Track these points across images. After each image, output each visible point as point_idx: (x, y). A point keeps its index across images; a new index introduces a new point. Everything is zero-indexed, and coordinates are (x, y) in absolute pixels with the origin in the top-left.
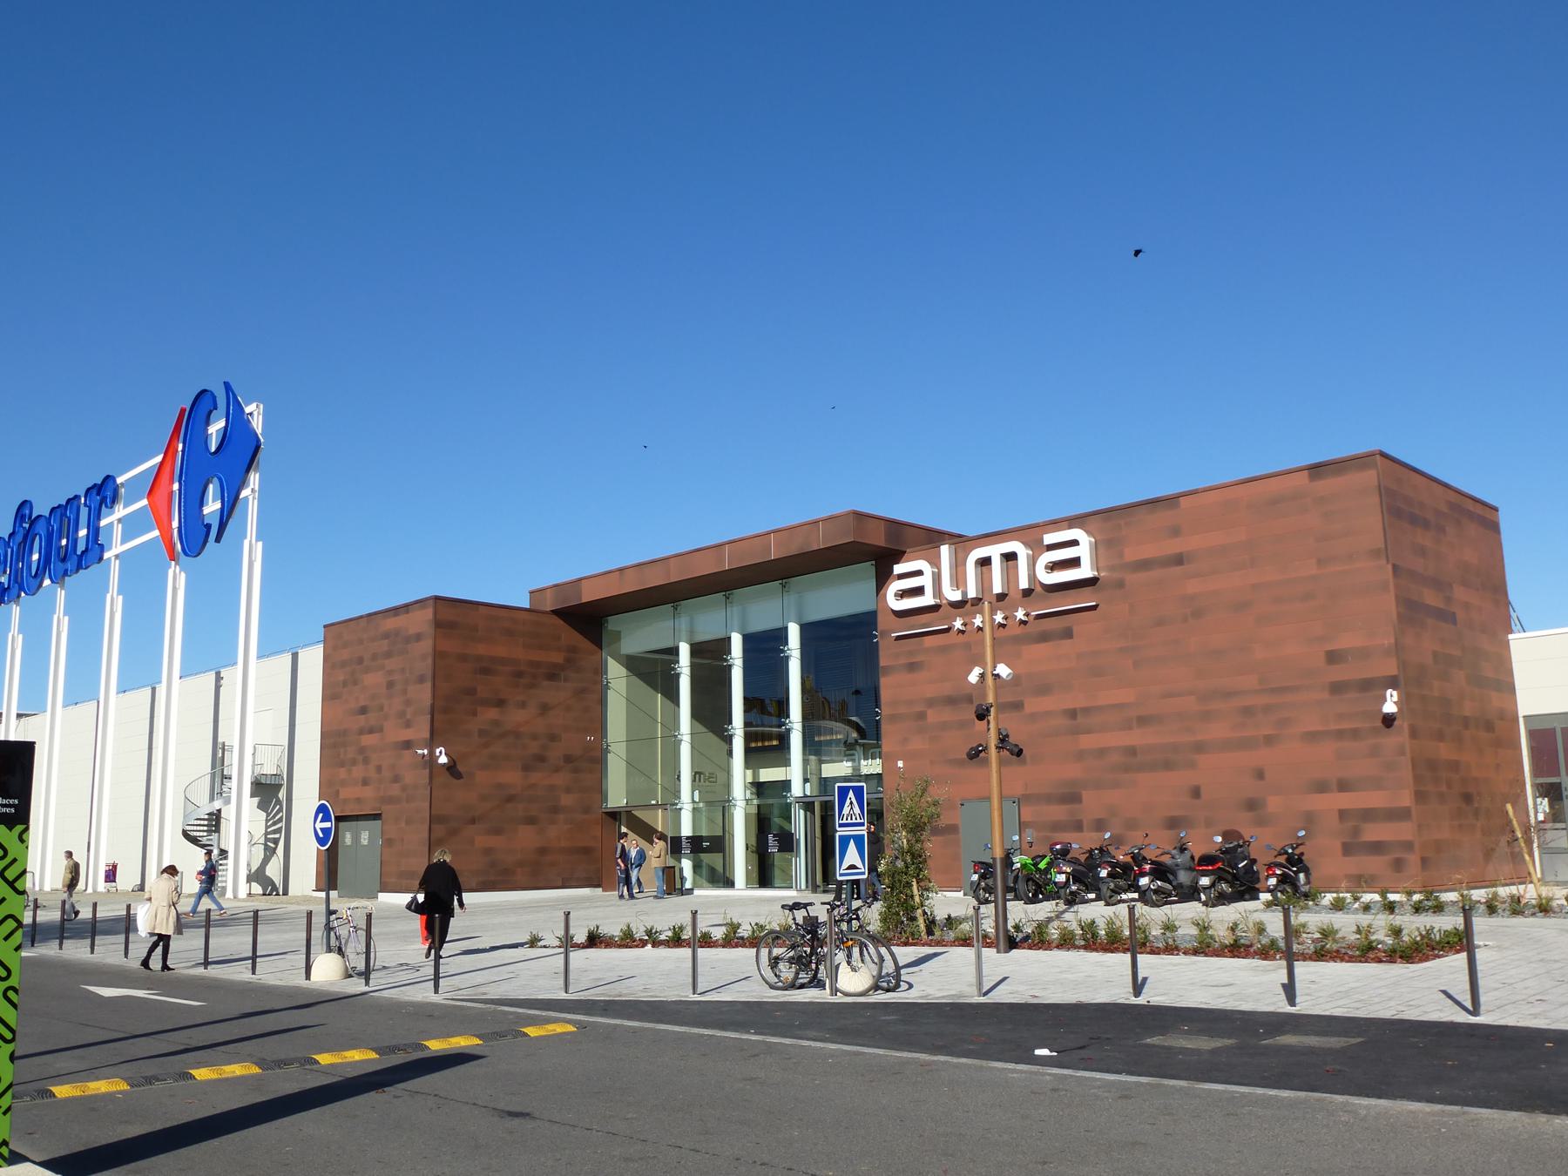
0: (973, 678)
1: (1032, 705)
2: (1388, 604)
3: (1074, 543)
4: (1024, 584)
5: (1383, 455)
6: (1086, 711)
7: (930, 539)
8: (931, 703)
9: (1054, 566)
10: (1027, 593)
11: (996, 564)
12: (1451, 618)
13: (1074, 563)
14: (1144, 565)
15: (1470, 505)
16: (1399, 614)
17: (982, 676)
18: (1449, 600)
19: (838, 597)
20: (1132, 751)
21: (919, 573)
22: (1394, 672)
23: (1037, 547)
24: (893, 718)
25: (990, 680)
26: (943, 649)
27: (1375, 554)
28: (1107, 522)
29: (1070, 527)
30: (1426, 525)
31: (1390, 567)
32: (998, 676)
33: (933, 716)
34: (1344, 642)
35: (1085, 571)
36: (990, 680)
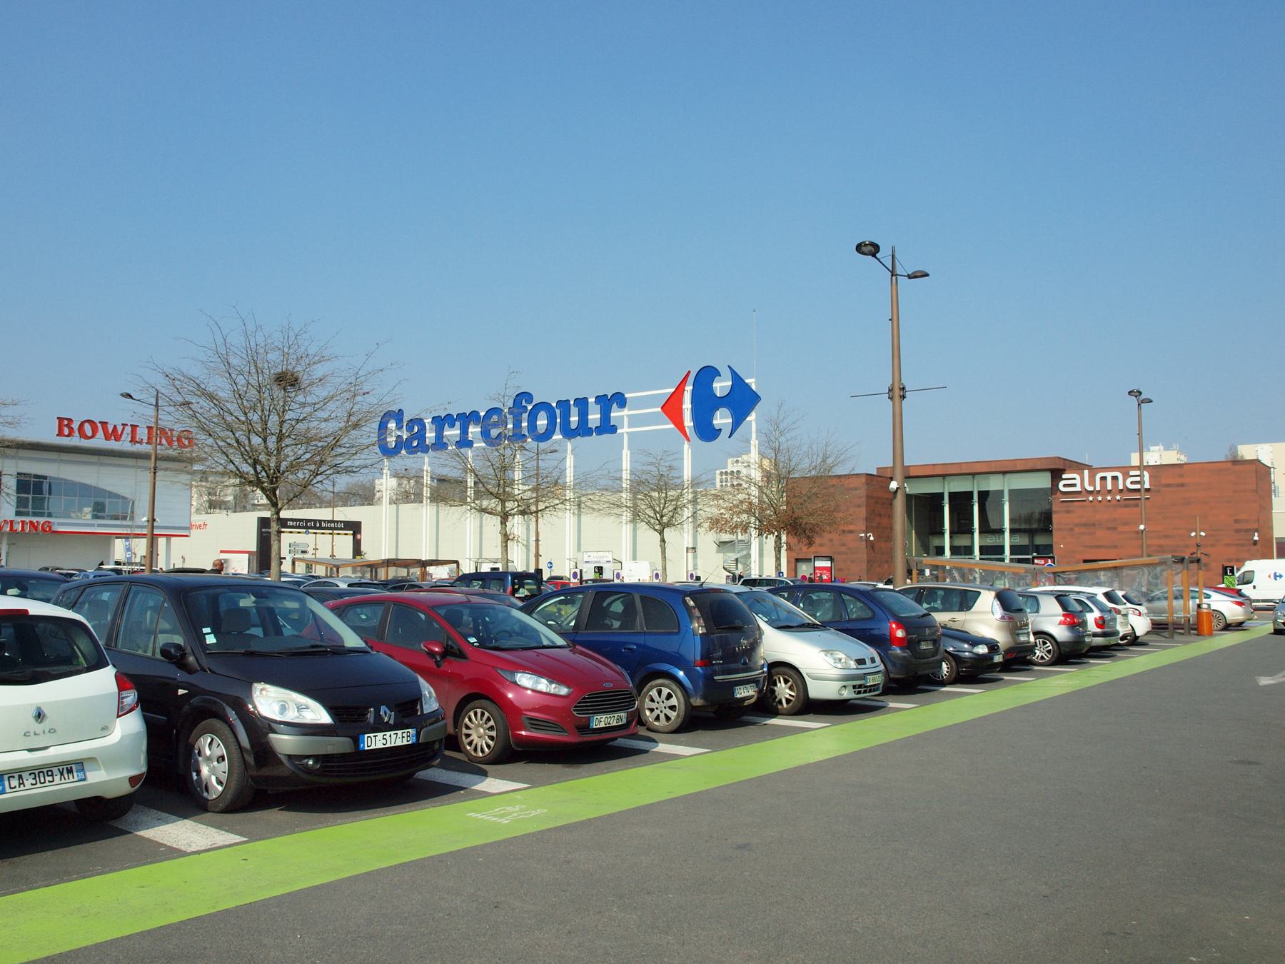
1: (1120, 529)
8: (1077, 525)
20: (1161, 546)
33: (1076, 530)
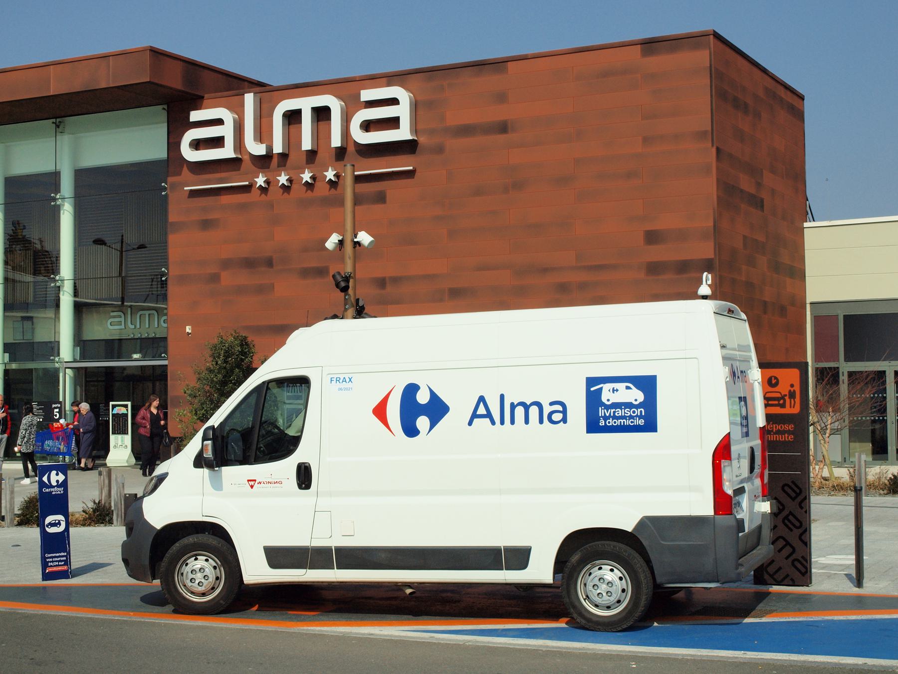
0: (332, 242)
2: (709, 187)
3: (394, 101)
4: (336, 141)
5: (717, 36)
6: (396, 280)
7: (232, 85)
8: (226, 264)
9: (367, 126)
10: (341, 153)
11: (307, 119)
12: (759, 203)
13: (393, 123)
14: (466, 130)
15: (782, 92)
16: (718, 197)
17: (341, 242)
18: (759, 185)
19: (132, 142)
21: (219, 122)
22: (710, 254)
23: (352, 105)
24: (182, 279)
25: (348, 247)
26: (243, 207)
27: (701, 135)
28: (425, 79)
29: (389, 85)
30: (745, 109)
31: (714, 150)
32: (358, 243)
34: (664, 222)
35: (403, 133)
36: (348, 247)
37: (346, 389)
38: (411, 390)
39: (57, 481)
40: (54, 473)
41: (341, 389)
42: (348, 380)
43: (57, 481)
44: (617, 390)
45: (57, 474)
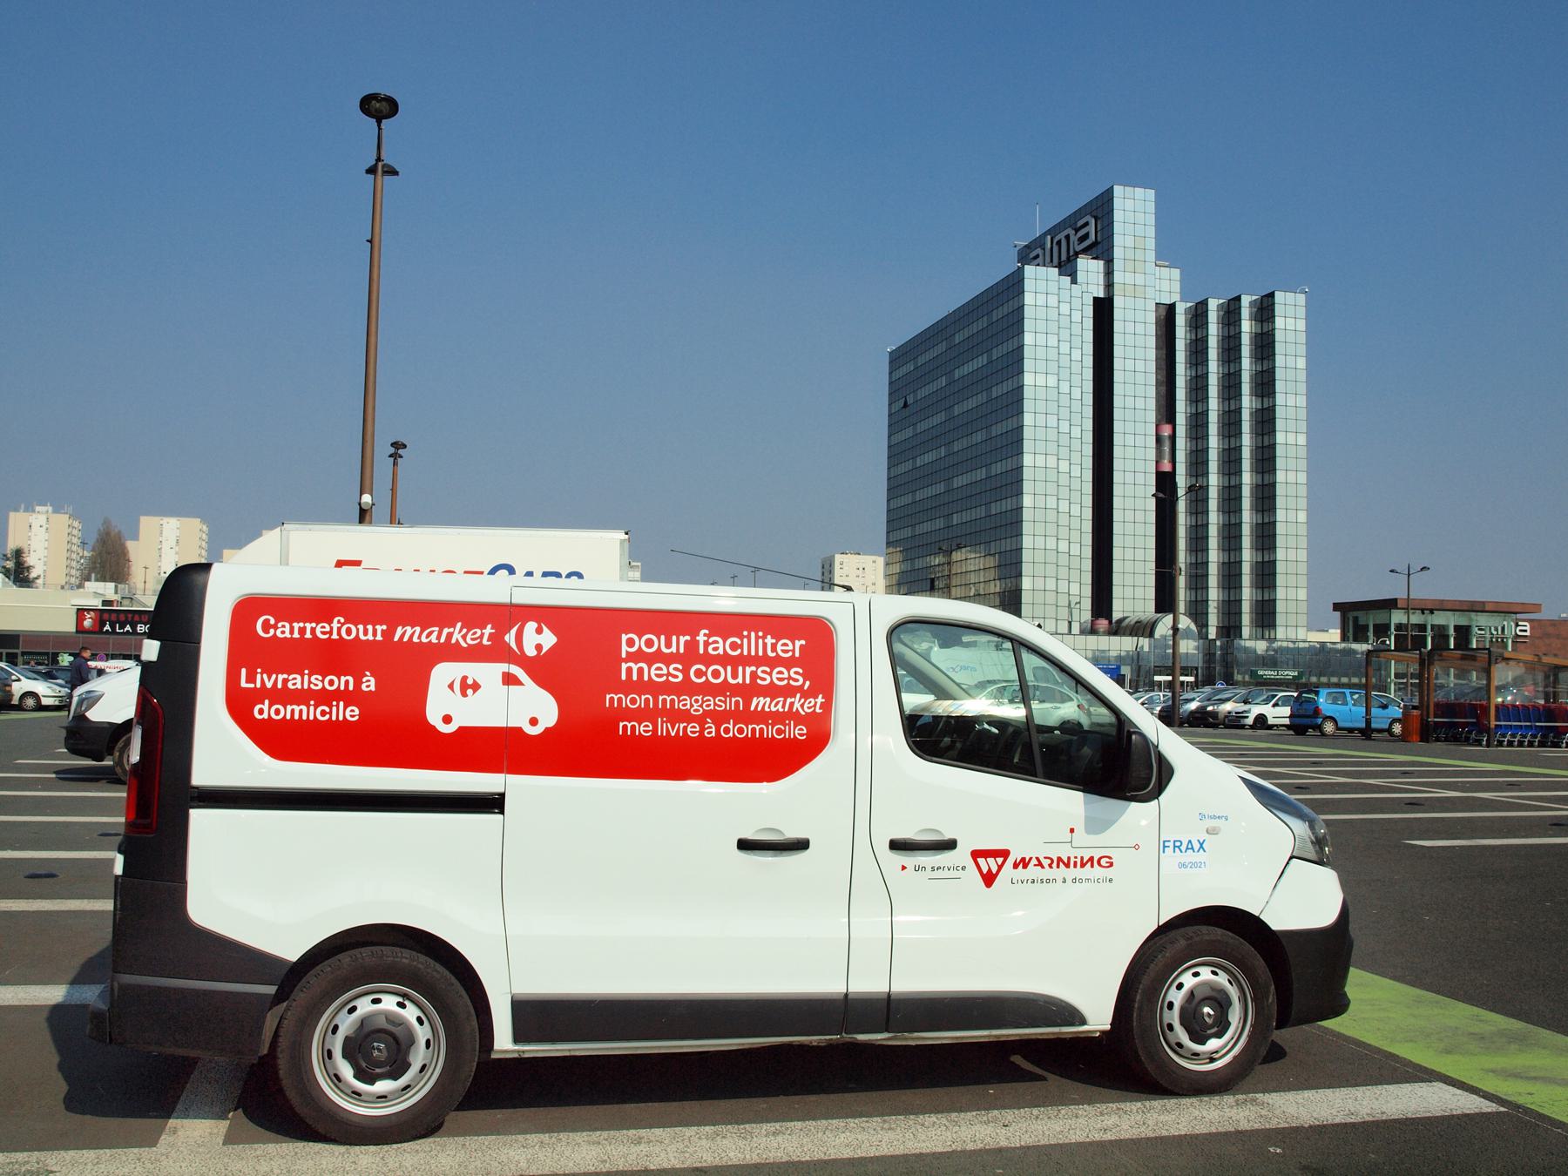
37: (1194, 865)
38: (465, 678)
39: (539, 647)
40: (531, 626)
41: (1183, 865)
42: (1196, 846)
43: (539, 647)
44: (476, 687)
45: (539, 631)
